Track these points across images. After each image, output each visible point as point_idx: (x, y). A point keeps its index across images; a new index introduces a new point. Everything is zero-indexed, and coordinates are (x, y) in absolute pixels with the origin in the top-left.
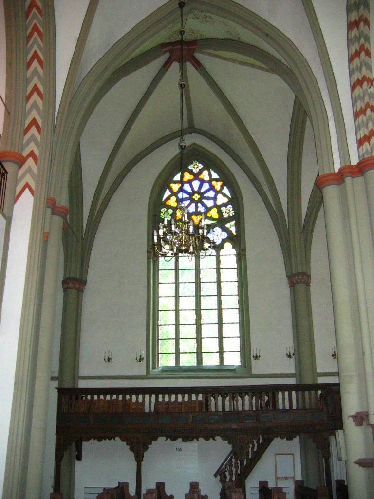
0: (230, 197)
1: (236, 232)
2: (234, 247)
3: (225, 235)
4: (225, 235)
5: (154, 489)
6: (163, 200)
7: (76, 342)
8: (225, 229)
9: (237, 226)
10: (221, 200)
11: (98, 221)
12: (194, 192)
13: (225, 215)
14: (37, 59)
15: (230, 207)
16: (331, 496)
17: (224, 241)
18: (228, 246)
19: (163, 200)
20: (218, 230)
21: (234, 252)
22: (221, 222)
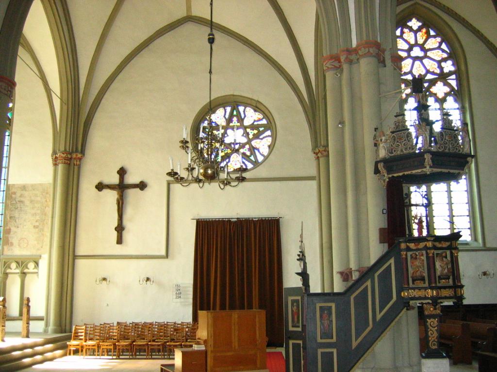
0: (449, 52)
1: (457, 86)
2: (456, 101)
3: (447, 89)
4: (447, 89)
5: (309, 292)
6: (437, 77)
7: (296, 92)
8: (446, 84)
9: (459, 80)
10: (438, 55)
11: (280, 11)
12: (425, 51)
13: (446, 70)
14: (422, 25)
15: (450, 62)
16: (288, 369)
17: (447, 94)
18: (450, 99)
19: (437, 77)
20: (440, 85)
21: (456, 106)
22: (443, 77)
